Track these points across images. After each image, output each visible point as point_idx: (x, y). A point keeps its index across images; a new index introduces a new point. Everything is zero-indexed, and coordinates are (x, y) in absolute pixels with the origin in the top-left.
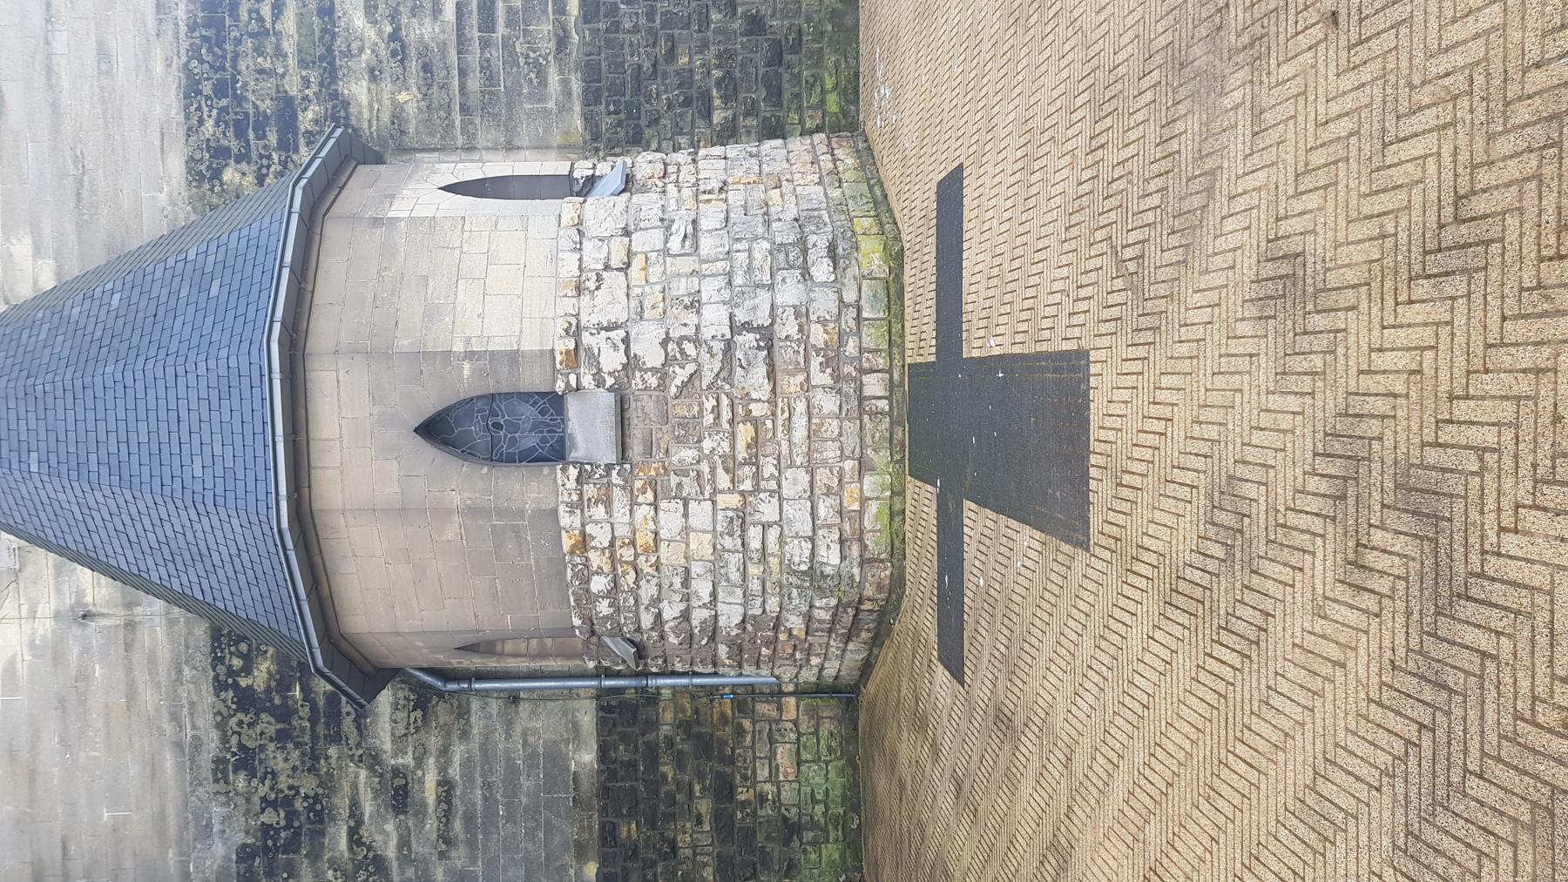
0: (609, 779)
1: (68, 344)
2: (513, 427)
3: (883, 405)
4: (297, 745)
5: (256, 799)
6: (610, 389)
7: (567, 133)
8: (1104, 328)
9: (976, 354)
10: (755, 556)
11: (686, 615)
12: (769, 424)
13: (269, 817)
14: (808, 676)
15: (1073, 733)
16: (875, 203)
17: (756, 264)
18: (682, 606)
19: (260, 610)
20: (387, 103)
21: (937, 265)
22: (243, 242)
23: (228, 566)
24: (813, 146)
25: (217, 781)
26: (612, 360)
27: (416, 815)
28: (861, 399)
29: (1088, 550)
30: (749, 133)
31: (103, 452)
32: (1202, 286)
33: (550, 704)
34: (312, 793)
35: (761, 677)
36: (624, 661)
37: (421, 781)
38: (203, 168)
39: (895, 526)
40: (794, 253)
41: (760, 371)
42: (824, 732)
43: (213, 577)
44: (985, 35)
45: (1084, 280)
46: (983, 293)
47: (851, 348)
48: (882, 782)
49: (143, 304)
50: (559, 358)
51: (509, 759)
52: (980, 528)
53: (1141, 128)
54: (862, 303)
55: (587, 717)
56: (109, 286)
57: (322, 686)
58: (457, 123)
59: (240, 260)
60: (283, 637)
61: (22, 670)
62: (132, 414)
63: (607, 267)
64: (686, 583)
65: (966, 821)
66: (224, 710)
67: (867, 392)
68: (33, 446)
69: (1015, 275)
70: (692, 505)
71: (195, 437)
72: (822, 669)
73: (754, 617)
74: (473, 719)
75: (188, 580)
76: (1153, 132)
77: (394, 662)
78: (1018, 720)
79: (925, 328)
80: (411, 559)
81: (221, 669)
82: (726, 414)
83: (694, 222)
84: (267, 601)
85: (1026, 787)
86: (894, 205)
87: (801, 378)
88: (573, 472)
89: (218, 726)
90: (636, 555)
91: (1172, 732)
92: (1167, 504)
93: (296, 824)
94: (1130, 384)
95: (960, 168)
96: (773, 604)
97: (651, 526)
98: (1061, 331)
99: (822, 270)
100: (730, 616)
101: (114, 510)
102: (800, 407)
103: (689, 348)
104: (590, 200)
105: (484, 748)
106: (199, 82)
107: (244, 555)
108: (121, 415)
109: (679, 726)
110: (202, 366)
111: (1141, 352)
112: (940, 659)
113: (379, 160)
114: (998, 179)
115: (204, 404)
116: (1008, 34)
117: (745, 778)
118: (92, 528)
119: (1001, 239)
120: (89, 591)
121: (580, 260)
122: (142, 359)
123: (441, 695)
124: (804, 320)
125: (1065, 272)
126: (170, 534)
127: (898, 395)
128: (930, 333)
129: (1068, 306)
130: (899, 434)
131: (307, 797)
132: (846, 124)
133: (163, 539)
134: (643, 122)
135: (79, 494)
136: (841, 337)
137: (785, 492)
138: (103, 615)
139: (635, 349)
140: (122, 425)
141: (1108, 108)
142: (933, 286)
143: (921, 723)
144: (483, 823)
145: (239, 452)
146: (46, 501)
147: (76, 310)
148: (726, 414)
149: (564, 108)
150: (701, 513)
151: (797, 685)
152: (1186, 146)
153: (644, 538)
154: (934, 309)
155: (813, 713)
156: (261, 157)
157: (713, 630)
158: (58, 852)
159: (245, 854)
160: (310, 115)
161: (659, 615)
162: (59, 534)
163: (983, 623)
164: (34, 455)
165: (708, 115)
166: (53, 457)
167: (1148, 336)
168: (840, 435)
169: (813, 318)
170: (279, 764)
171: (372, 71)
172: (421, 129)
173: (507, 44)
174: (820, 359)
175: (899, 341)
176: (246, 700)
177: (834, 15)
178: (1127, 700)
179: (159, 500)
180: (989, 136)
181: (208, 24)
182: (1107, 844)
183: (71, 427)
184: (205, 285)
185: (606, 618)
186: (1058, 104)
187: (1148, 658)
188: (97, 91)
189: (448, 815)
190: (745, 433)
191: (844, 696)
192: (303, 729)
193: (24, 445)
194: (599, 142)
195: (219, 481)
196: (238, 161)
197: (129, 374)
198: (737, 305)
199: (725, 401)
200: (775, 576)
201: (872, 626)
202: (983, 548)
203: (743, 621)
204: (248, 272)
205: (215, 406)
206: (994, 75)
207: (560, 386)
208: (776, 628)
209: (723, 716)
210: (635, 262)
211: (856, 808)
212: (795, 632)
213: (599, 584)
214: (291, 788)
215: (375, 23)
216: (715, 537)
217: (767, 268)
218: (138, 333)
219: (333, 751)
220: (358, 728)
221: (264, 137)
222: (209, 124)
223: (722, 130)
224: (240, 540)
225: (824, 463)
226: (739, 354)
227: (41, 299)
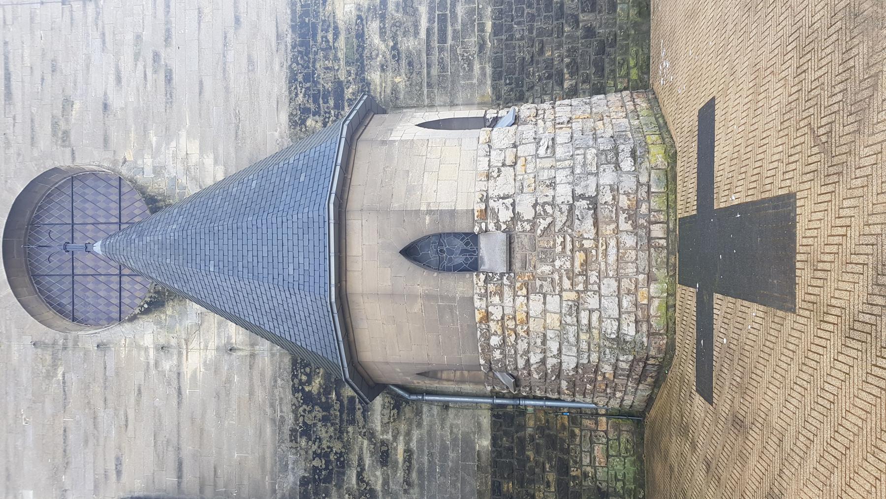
0: (497, 457)
1: (230, 206)
2: (451, 252)
3: (663, 242)
4: (332, 424)
5: (310, 452)
6: (504, 231)
7: (483, 96)
8: (805, 178)
9: (722, 205)
10: (585, 328)
11: (543, 361)
12: (594, 252)
13: (317, 463)
14: (614, 404)
15: (784, 425)
16: (660, 128)
17: (588, 162)
18: (541, 356)
19: (318, 347)
20: (389, 83)
21: (698, 158)
22: (317, 154)
23: (304, 322)
24: (622, 98)
25: (291, 441)
26: (505, 215)
27: (392, 468)
28: (650, 239)
29: (794, 312)
30: (584, 92)
31: (245, 261)
32: (870, 143)
33: (466, 411)
34: (339, 451)
35: (585, 403)
36: (507, 388)
37: (396, 449)
38: (297, 119)
39: (670, 314)
40: (611, 155)
41: (590, 221)
42: (623, 438)
43: (296, 328)
44: (729, 21)
45: (793, 151)
46: (728, 169)
47: (644, 209)
48: (659, 469)
49: (267, 186)
50: (476, 214)
51: (443, 440)
52: (724, 309)
53: (829, 57)
54: (651, 183)
55: (486, 420)
56: (251, 177)
57: (348, 392)
58: (425, 92)
59: (315, 162)
60: (329, 361)
61: (200, 376)
62: (260, 241)
63: (504, 165)
64: (544, 343)
65: (713, 486)
66: (296, 403)
67: (653, 234)
68: (212, 258)
69: (748, 155)
70: (548, 297)
71: (291, 254)
72: (622, 400)
73: (583, 364)
74: (424, 417)
75: (282, 330)
76: (837, 57)
77: (384, 380)
78: (747, 422)
79: (690, 195)
80: (397, 325)
81: (296, 381)
82: (569, 246)
83: (553, 139)
84: (322, 342)
85: (753, 461)
86: (671, 128)
87: (613, 226)
88: (482, 277)
89: (293, 412)
90: (516, 325)
91: (850, 417)
92: (846, 277)
93: (330, 467)
94: (823, 209)
95: (713, 99)
96: (594, 357)
97: (525, 308)
98: (778, 184)
99: (627, 164)
100: (569, 363)
101: (249, 291)
102: (613, 243)
103: (549, 209)
104: (495, 129)
105: (429, 432)
106: (296, 75)
107: (312, 316)
108: (255, 242)
109: (538, 429)
110: (295, 217)
111: (830, 188)
112: (697, 391)
113: (384, 112)
114: (737, 101)
115: (296, 237)
116: (744, 17)
117: (576, 462)
118: (238, 301)
119: (739, 136)
120: (234, 337)
121: (489, 161)
122: (266, 213)
123: (407, 402)
124: (615, 193)
125: (780, 148)
126: (276, 305)
127: (672, 237)
128: (693, 198)
129: (782, 167)
130: (672, 260)
131: (336, 453)
132: (642, 84)
133: (272, 307)
134: (525, 88)
135: (233, 283)
136: (638, 203)
137: (603, 292)
138: (239, 349)
139: (518, 209)
140: (255, 247)
141: (808, 49)
142: (696, 170)
143: (684, 430)
144: (428, 476)
145: (312, 262)
146: (216, 286)
147: (235, 189)
148: (569, 246)
149: (481, 83)
150: (553, 302)
151: (607, 410)
152: (859, 63)
153: (521, 316)
154: (696, 183)
155: (617, 427)
156: (326, 113)
157: (558, 370)
158: (212, 473)
159: (304, 482)
160: (350, 90)
161: (528, 360)
162: (222, 304)
163: (726, 365)
164: (212, 262)
165: (561, 84)
166: (221, 263)
167: (835, 178)
168: (637, 259)
169: (621, 192)
170: (323, 434)
171: (382, 66)
172: (406, 96)
173: (453, 49)
174: (625, 215)
175: (673, 205)
176: (308, 398)
177: (636, 25)
178: (820, 400)
179: (271, 287)
180: (732, 78)
181: (302, 44)
182: (806, 489)
183: (230, 248)
184: (298, 176)
185: (498, 361)
186: (776, 52)
187: (834, 372)
188: (247, 80)
189: (409, 469)
190: (580, 257)
191: (635, 418)
192: (336, 416)
193: (207, 257)
194: (500, 100)
195: (301, 277)
196: (314, 115)
197: (259, 221)
198: (577, 185)
199: (568, 238)
200: (596, 341)
201: (654, 374)
202: (726, 321)
203: (577, 367)
204: (319, 169)
205: (301, 238)
206: (735, 43)
207: (476, 229)
208: (596, 372)
209: (563, 424)
210: (519, 162)
211: (642, 486)
212: (607, 376)
213: (495, 341)
214: (328, 447)
215: (384, 41)
216: (561, 317)
217: (594, 164)
218: (264, 201)
219: (350, 429)
220: (364, 417)
221: (327, 102)
222: (301, 96)
223: (569, 91)
224: (310, 308)
225: (627, 276)
226: (577, 212)
227: (217, 185)
